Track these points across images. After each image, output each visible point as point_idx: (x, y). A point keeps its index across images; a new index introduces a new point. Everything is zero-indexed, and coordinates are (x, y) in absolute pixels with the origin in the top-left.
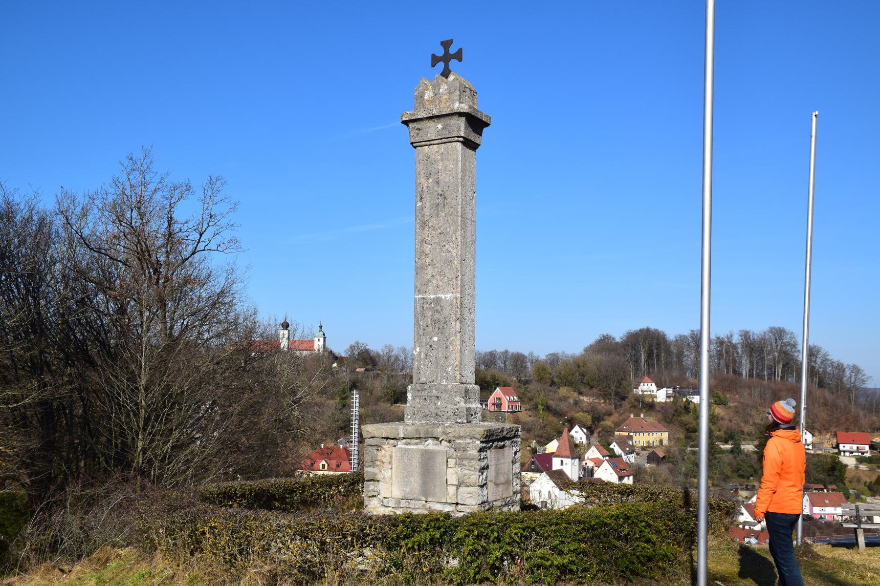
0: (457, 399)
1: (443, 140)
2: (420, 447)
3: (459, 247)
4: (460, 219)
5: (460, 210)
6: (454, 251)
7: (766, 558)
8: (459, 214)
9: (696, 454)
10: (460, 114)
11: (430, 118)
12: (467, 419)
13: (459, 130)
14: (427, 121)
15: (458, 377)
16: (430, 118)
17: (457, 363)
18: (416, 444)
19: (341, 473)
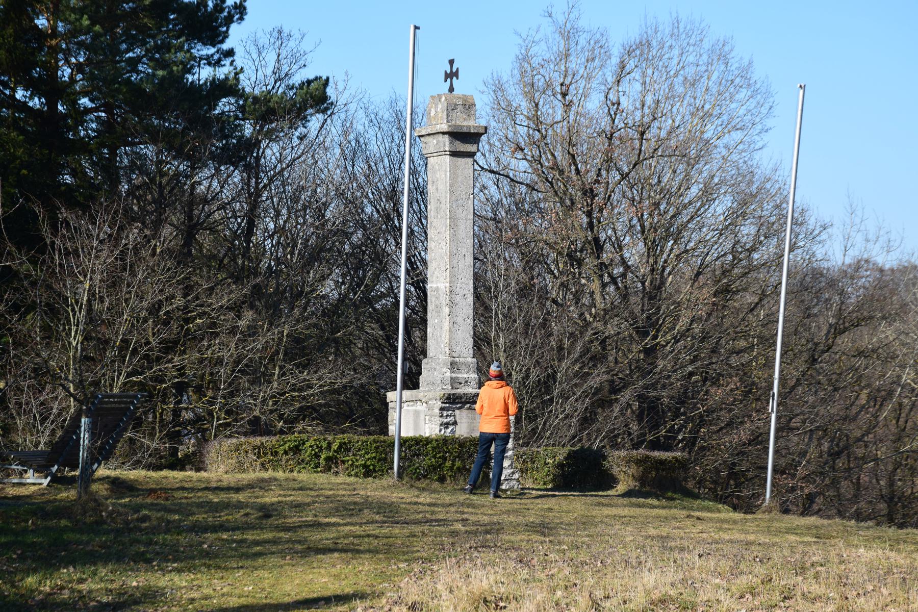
0: (444, 370)
1: (439, 154)
2: (414, 408)
3: (448, 245)
4: (448, 220)
5: (448, 213)
6: (444, 248)
7: (261, 598)
8: (448, 216)
9: (771, 376)
10: (443, 133)
11: (429, 135)
12: (452, 385)
13: (445, 146)
14: (428, 137)
15: (448, 352)
16: (429, 135)
17: (447, 341)
18: (412, 406)
19: (120, 501)
